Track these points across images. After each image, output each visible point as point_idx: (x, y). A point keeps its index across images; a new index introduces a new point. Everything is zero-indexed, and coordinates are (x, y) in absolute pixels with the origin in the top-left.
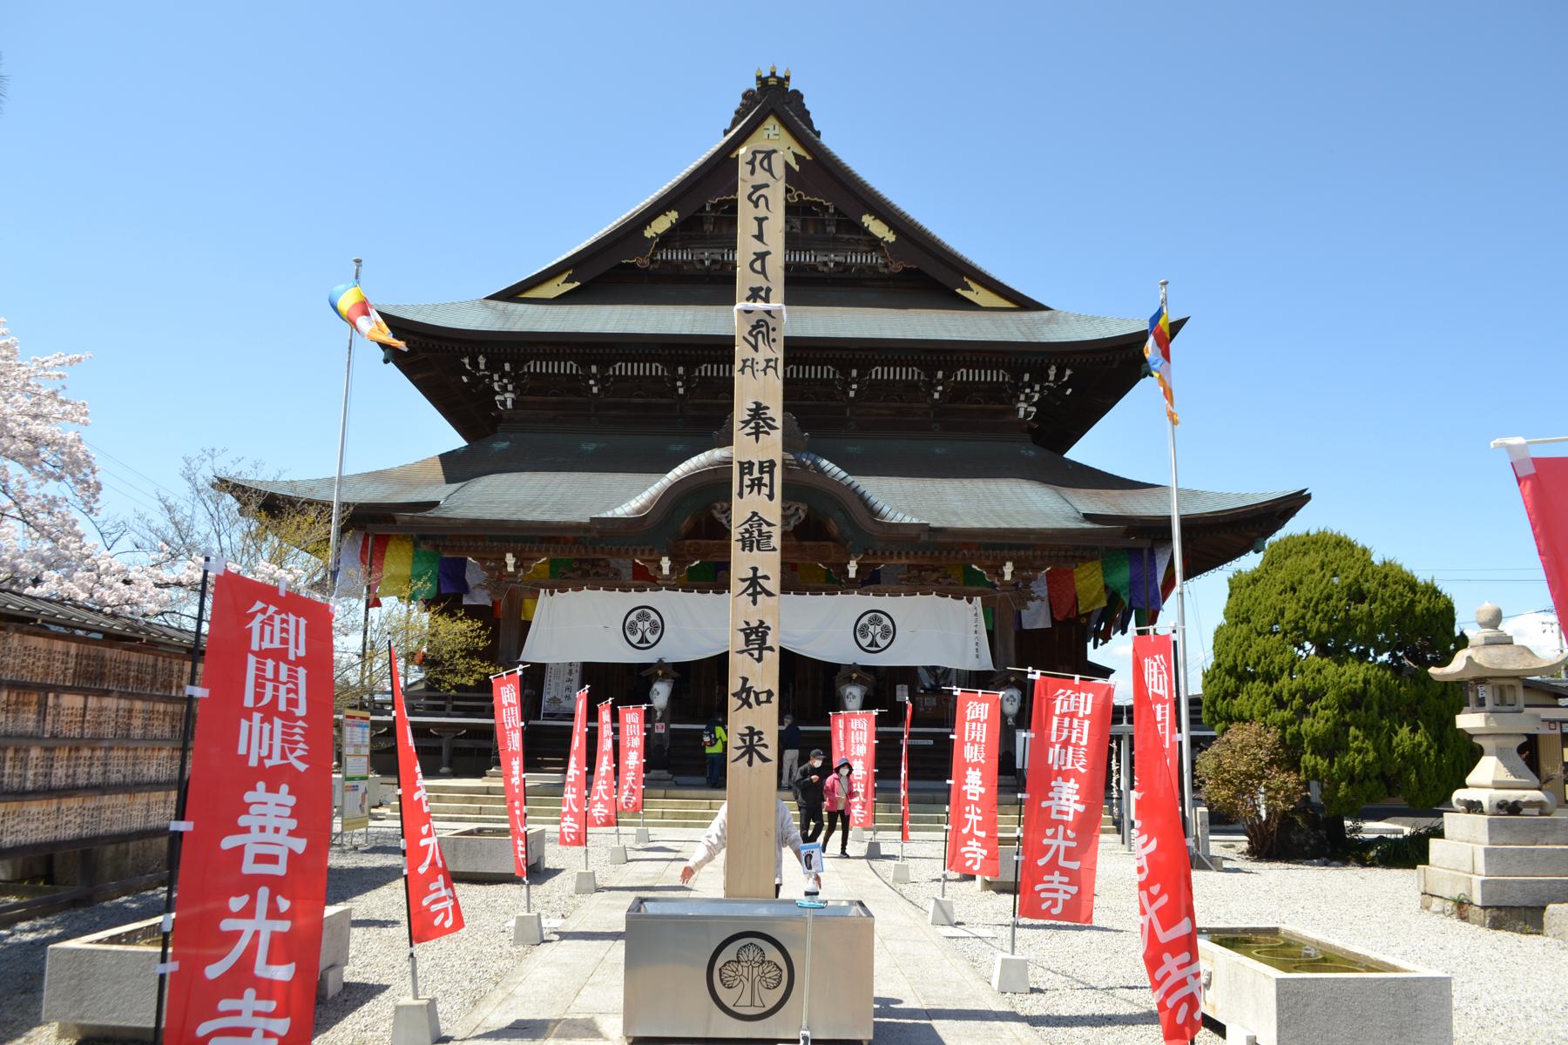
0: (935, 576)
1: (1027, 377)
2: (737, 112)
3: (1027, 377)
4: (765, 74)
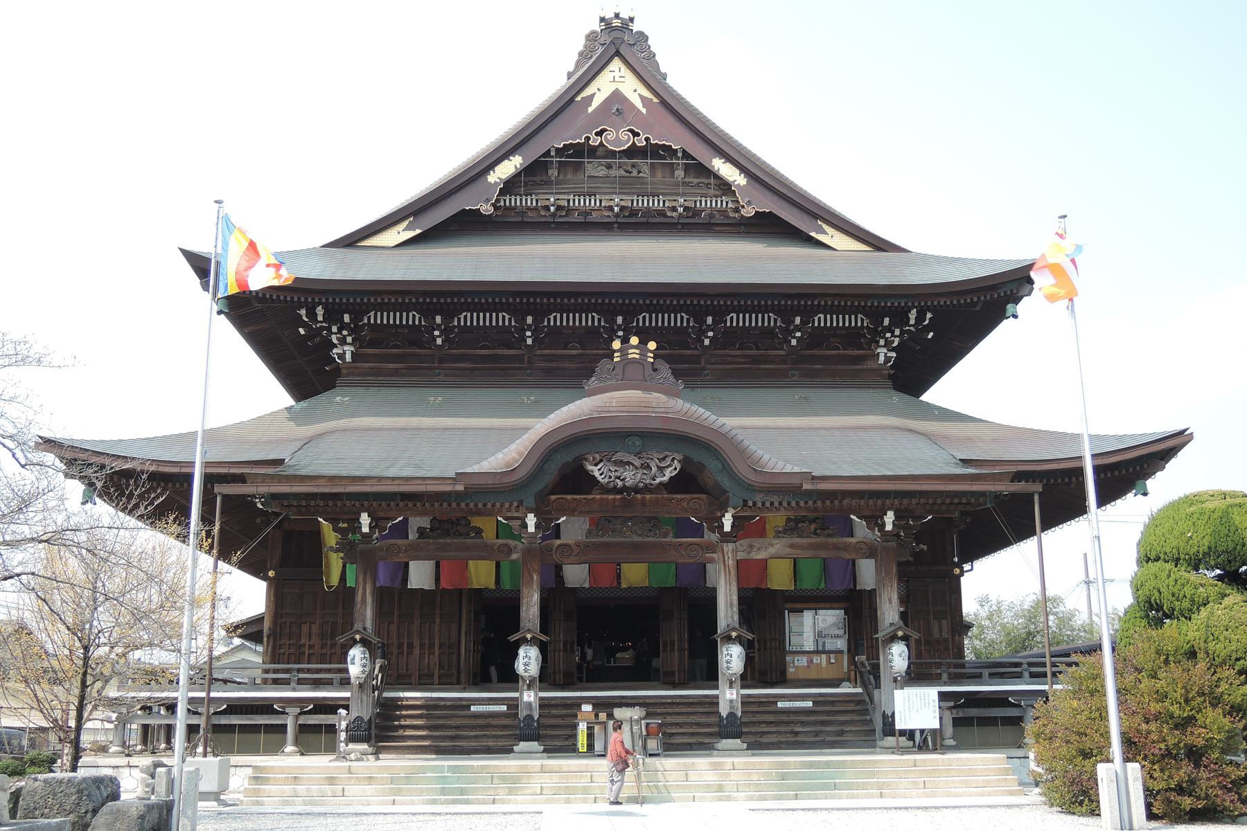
0: (813, 527)
1: (886, 321)
2: (581, 54)
3: (886, 321)
4: (609, 15)
